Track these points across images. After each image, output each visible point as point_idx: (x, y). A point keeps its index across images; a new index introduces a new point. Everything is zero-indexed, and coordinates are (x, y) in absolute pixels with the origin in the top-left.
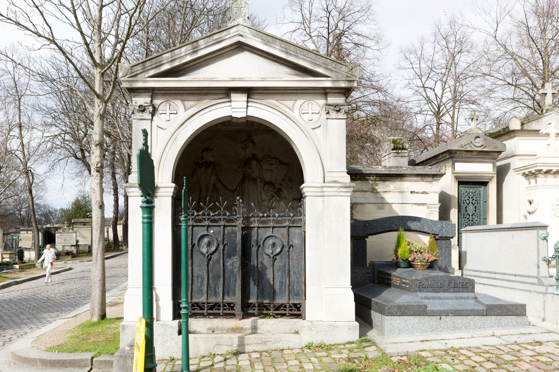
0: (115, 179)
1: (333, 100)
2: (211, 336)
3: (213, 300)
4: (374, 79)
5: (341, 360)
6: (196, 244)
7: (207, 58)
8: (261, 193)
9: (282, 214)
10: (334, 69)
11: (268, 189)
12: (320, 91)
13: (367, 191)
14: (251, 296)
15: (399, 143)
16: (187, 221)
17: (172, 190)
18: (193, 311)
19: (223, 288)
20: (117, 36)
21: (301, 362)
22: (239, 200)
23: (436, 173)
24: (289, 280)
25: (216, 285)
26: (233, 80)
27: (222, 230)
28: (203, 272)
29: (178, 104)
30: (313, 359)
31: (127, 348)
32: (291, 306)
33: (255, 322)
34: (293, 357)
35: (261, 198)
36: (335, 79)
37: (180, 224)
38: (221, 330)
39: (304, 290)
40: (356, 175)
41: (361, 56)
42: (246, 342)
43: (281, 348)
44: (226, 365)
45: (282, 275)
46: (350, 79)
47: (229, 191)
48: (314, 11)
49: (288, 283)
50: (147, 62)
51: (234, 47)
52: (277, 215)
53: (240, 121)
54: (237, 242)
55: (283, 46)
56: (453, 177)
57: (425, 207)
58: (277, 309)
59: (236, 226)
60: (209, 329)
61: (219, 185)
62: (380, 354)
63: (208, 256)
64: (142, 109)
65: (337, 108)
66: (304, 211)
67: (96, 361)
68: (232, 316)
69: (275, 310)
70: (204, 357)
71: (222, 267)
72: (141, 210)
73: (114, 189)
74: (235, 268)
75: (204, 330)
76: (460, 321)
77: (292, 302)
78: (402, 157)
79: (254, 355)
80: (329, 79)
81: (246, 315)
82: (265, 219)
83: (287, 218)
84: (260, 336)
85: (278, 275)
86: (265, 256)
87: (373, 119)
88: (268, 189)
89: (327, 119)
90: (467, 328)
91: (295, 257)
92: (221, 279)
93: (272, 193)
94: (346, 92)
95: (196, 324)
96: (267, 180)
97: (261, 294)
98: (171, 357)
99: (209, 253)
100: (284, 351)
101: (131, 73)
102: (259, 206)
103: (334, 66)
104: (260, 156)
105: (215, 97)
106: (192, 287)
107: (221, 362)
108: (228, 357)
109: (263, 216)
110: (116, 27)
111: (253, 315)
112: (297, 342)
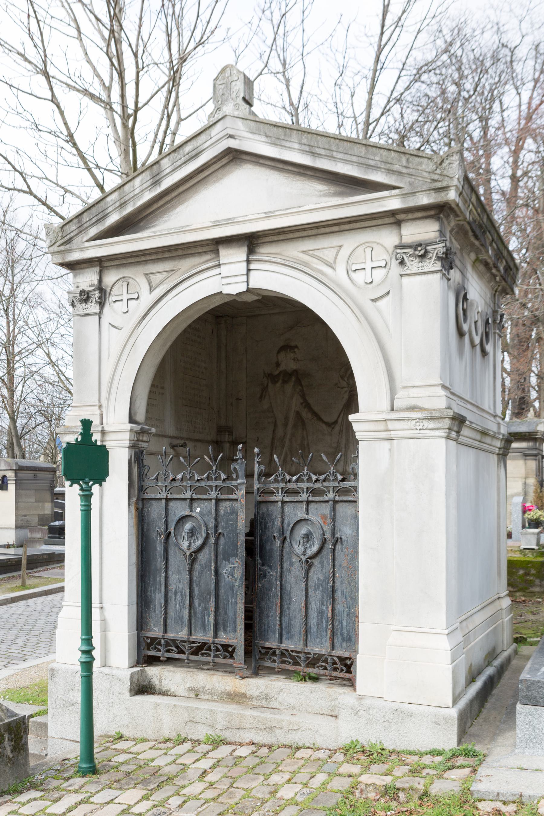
3: (199, 636)
10: (404, 171)
24: (333, 610)
25: (205, 609)
26: (217, 224)
27: (214, 507)
32: (334, 663)
45: (323, 598)
46: (439, 185)
47: (324, 426)
50: (85, 215)
55: (305, 141)
59: (236, 500)
60: (190, 690)
61: (305, 414)
65: (420, 250)
67: (34, 722)
89: (401, 275)
91: (345, 564)
92: (213, 599)
98: (118, 733)
99: (192, 550)
101: (63, 237)
103: (404, 163)
109: (317, 481)
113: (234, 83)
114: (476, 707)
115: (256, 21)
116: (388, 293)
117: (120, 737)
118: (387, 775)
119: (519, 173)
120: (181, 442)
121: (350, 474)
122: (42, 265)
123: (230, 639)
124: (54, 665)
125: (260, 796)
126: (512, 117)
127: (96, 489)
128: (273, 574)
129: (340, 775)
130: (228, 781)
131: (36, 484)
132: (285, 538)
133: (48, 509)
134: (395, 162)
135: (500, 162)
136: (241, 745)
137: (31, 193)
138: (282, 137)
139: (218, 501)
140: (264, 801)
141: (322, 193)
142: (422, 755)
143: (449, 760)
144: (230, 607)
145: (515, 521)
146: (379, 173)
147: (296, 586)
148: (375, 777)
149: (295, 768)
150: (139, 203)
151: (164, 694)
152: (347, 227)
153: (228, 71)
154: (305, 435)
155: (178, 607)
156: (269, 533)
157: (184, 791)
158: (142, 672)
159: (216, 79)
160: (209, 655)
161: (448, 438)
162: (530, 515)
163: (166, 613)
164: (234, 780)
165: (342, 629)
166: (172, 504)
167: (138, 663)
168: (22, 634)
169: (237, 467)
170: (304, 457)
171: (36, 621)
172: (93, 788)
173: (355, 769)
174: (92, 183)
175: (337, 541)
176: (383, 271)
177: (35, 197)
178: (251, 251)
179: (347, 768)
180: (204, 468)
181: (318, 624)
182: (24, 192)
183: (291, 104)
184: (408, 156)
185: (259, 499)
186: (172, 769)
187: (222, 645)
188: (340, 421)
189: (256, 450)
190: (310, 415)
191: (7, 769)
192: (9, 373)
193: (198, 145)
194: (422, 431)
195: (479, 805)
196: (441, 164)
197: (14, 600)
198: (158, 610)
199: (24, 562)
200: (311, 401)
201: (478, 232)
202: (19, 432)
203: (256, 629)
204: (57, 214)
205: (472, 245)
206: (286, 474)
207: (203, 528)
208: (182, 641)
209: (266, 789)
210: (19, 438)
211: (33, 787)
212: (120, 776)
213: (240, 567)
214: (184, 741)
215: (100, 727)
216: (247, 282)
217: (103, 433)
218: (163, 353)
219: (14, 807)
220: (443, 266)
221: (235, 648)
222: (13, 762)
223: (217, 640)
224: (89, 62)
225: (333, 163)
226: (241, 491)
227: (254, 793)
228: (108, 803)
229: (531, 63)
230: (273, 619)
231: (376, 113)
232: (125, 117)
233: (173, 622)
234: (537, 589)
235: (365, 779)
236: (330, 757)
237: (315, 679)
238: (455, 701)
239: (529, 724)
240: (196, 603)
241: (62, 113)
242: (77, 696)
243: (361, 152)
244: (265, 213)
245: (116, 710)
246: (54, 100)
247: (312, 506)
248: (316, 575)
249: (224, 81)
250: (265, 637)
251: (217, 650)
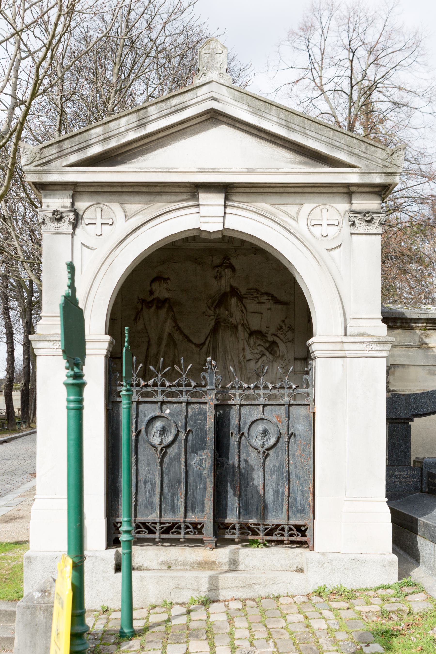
0: (9, 317)
1: (361, 203)
2: (167, 575)
3: (169, 518)
4: (423, 160)
5: (371, 614)
6: (143, 431)
7: (160, 135)
8: (243, 349)
9: (278, 385)
10: (363, 155)
11: (255, 343)
12: (341, 190)
13: (411, 347)
14: (229, 512)
16: (129, 396)
17: (106, 345)
18: (138, 536)
19: (186, 500)
20: (14, 96)
21: (307, 618)
22: (210, 362)
24: (289, 489)
25: (175, 494)
26: (202, 171)
27: (184, 409)
28: (154, 475)
29: (114, 208)
30: (326, 613)
31: (37, 595)
32: (291, 529)
33: (234, 554)
34: (295, 609)
35: (244, 356)
36: (365, 170)
37: (118, 399)
38: (181, 565)
39: (312, 505)
40: (393, 321)
41: (403, 123)
42: (221, 584)
43: (276, 595)
44: (191, 620)
46: (389, 170)
47: (193, 346)
48: (328, 50)
49: (286, 493)
50: (66, 142)
51: (203, 118)
53: (213, 237)
54: (207, 428)
55: (282, 116)
58: (270, 533)
59: (206, 403)
60: (163, 563)
61: (177, 336)
62: (431, 607)
63: (162, 450)
64: (58, 217)
65: (368, 217)
66: (314, 379)
68: (201, 542)
69: (266, 535)
70: (154, 607)
71: (183, 467)
72: (64, 388)
73: (6, 334)
74: (204, 469)
75: (154, 565)
77: (294, 521)
79: (234, 605)
80: (355, 170)
81: (221, 541)
82: (251, 391)
83: (286, 391)
84: (244, 575)
85: (271, 480)
86: (251, 450)
87: (421, 225)
88: (255, 343)
89: (351, 234)
92: (183, 485)
93: (262, 348)
94: (383, 191)
95: (143, 555)
96: (254, 327)
97: (245, 509)
98: (103, 607)
99: (163, 445)
100: (281, 599)
101: (40, 159)
102: (241, 369)
103: (364, 150)
104: (243, 291)
105: (173, 198)
106: (136, 497)
107: (182, 615)
108: (192, 607)
110: (14, 79)
111: (232, 542)
112: (302, 585)
113: (218, 55)
116: (340, 246)
123: (198, 518)
134: (356, 147)
138: (263, 110)
141: (289, 160)
144: (198, 491)
146: (342, 153)
154: (176, 353)
155: (150, 494)
165: (296, 503)
169: (205, 375)
181: (274, 501)
184: (366, 144)
187: (190, 523)
188: (207, 343)
190: (181, 337)
193: (185, 100)
194: (370, 352)
196: (391, 155)
200: (181, 325)
206: (141, 380)
208: (153, 523)
213: (209, 457)
216: (224, 223)
221: (203, 525)
225: (305, 138)
226: (210, 395)
233: (143, 507)
240: (166, 489)
243: (330, 134)
244: (247, 169)
249: (209, 52)
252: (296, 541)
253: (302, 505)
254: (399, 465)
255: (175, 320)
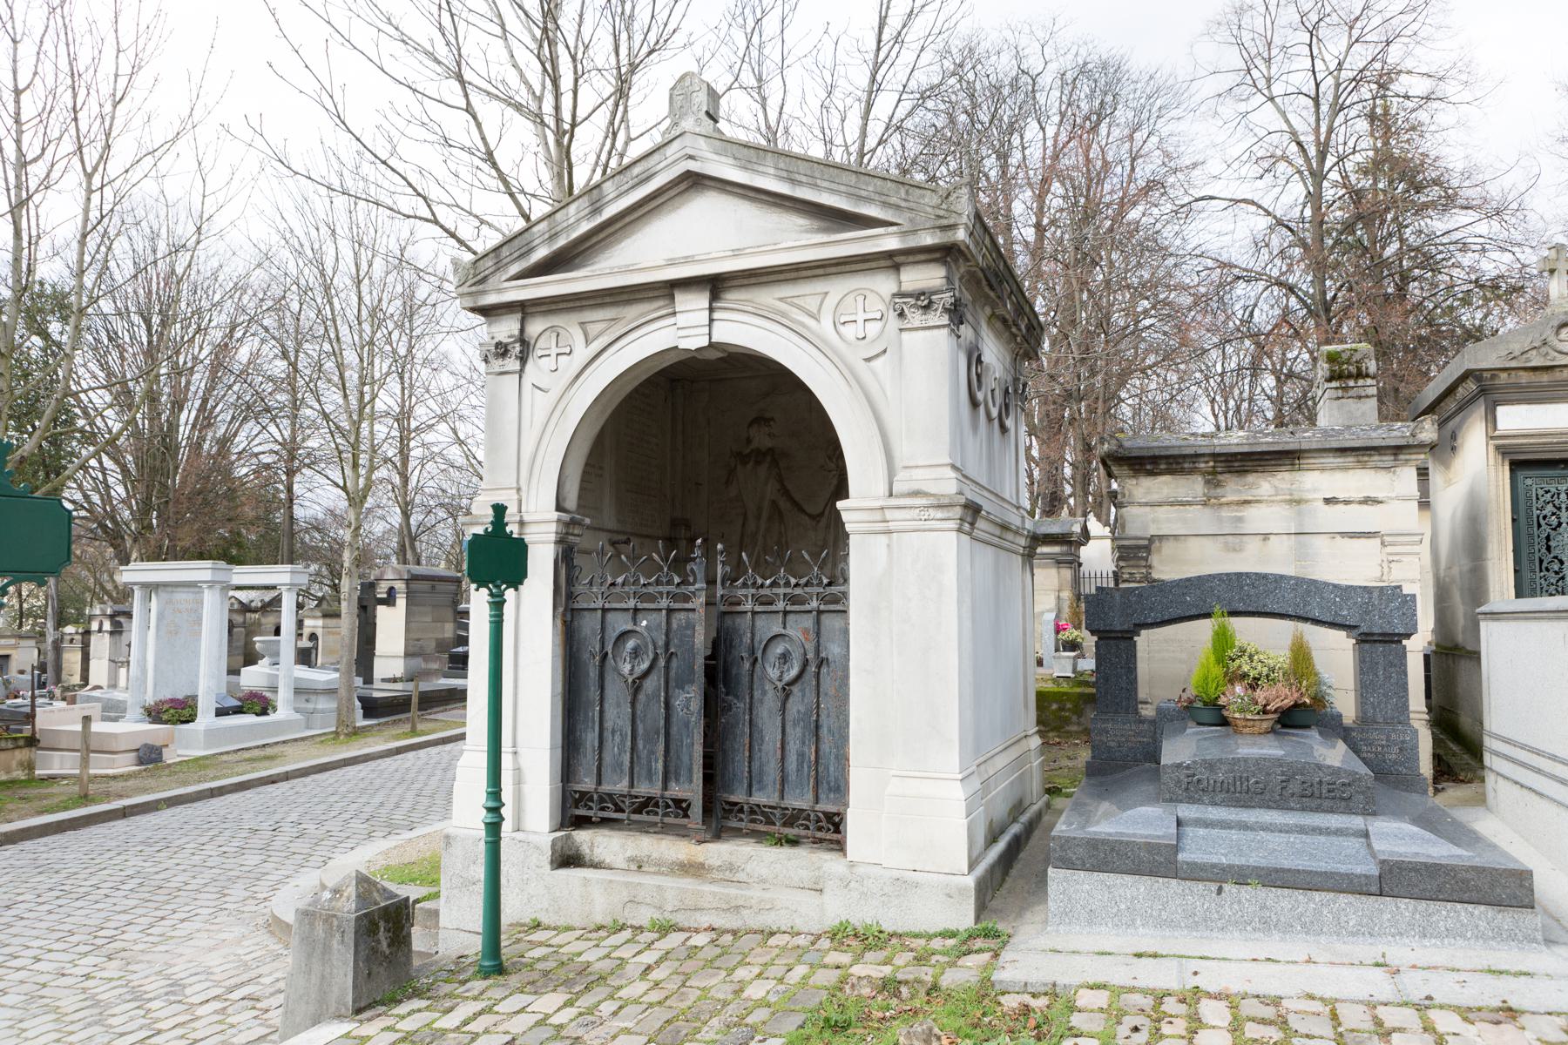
3: (643, 789)
5: (865, 982)
10: (903, 204)
13: (1189, 504)
15: (1348, 362)
19: (665, 762)
23: (1402, 442)
24: (817, 752)
25: (652, 752)
26: (672, 263)
36: (907, 227)
46: (945, 222)
52: (793, 581)
55: (782, 165)
56: (1491, 449)
57: (1378, 541)
60: (631, 860)
65: (924, 300)
76: (1285, 904)
78: (1360, 397)
80: (894, 229)
90: (1310, 928)
91: (832, 692)
109: (797, 585)
114: (998, 875)
115: (724, 26)
117: (537, 926)
118: (885, 964)
119: (1045, 221)
120: (624, 538)
121: (837, 575)
122: (449, 317)
124: (451, 831)
125: (721, 996)
126: (1035, 154)
127: (510, 594)
128: (740, 706)
129: (825, 966)
130: (679, 979)
131: (436, 598)
132: (756, 660)
133: (448, 631)
135: (1021, 206)
136: (697, 931)
137: (436, 222)
139: (670, 611)
140: (725, 1003)
142: (930, 937)
143: (964, 942)
145: (1045, 642)
147: (769, 722)
148: (871, 968)
149: (766, 959)
150: (575, 235)
151: (596, 866)
152: (833, 270)
153: (688, 80)
155: (617, 750)
156: (735, 653)
157: (621, 993)
158: (568, 837)
159: (673, 89)
160: (656, 814)
161: (959, 530)
162: (1064, 636)
163: (600, 759)
164: (687, 976)
166: (610, 616)
167: (562, 826)
168: (410, 796)
170: (780, 555)
171: (429, 777)
172: (497, 993)
173: (845, 958)
174: (516, 212)
175: (822, 662)
176: (879, 325)
177: (442, 227)
178: (715, 297)
179: (834, 957)
180: (651, 568)
182: (427, 220)
183: (768, 127)
185: (723, 608)
186: (606, 965)
189: (719, 546)
191: (382, 970)
192: (401, 452)
195: (1002, 999)
197: (399, 751)
198: (589, 756)
199: (415, 700)
200: (789, 487)
201: (993, 281)
202: (414, 530)
203: (718, 778)
204: (469, 249)
205: (987, 297)
207: (651, 647)
209: (729, 988)
210: (413, 539)
211: (417, 994)
212: (535, 976)
214: (622, 928)
215: (510, 911)
217: (522, 523)
218: (602, 422)
219: (389, 1022)
220: (951, 319)
222: (390, 961)
223: (667, 794)
224: (515, 66)
227: (713, 993)
228: (518, 1012)
229: (1056, 93)
230: (739, 763)
231: (871, 142)
232: (559, 133)
234: (1074, 728)
235: (857, 970)
236: (813, 944)
237: (794, 842)
238: (971, 867)
239: (1063, 893)
240: (640, 744)
241: (479, 125)
242: (480, 872)
245: (534, 888)
246: (469, 109)
247: (791, 617)
248: (795, 706)
250: (729, 788)
251: (668, 806)
252: (1223, 828)
253: (836, 780)
254: (1116, 712)
255: (781, 480)
